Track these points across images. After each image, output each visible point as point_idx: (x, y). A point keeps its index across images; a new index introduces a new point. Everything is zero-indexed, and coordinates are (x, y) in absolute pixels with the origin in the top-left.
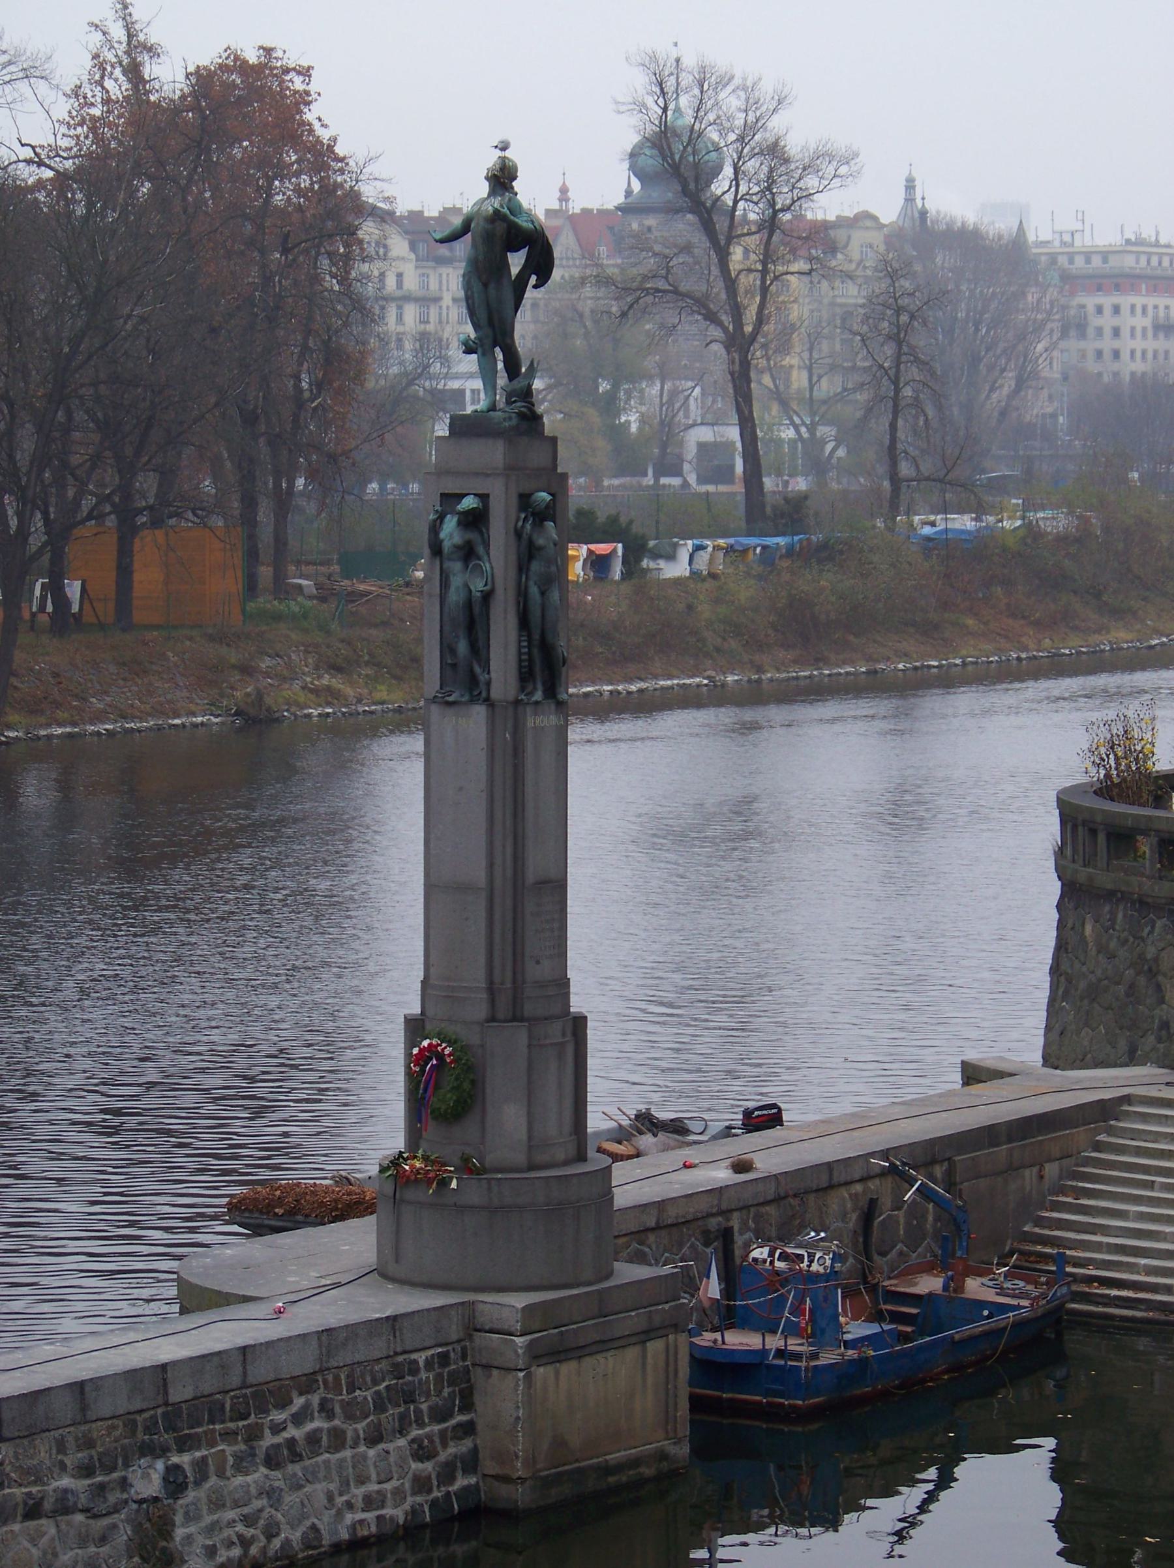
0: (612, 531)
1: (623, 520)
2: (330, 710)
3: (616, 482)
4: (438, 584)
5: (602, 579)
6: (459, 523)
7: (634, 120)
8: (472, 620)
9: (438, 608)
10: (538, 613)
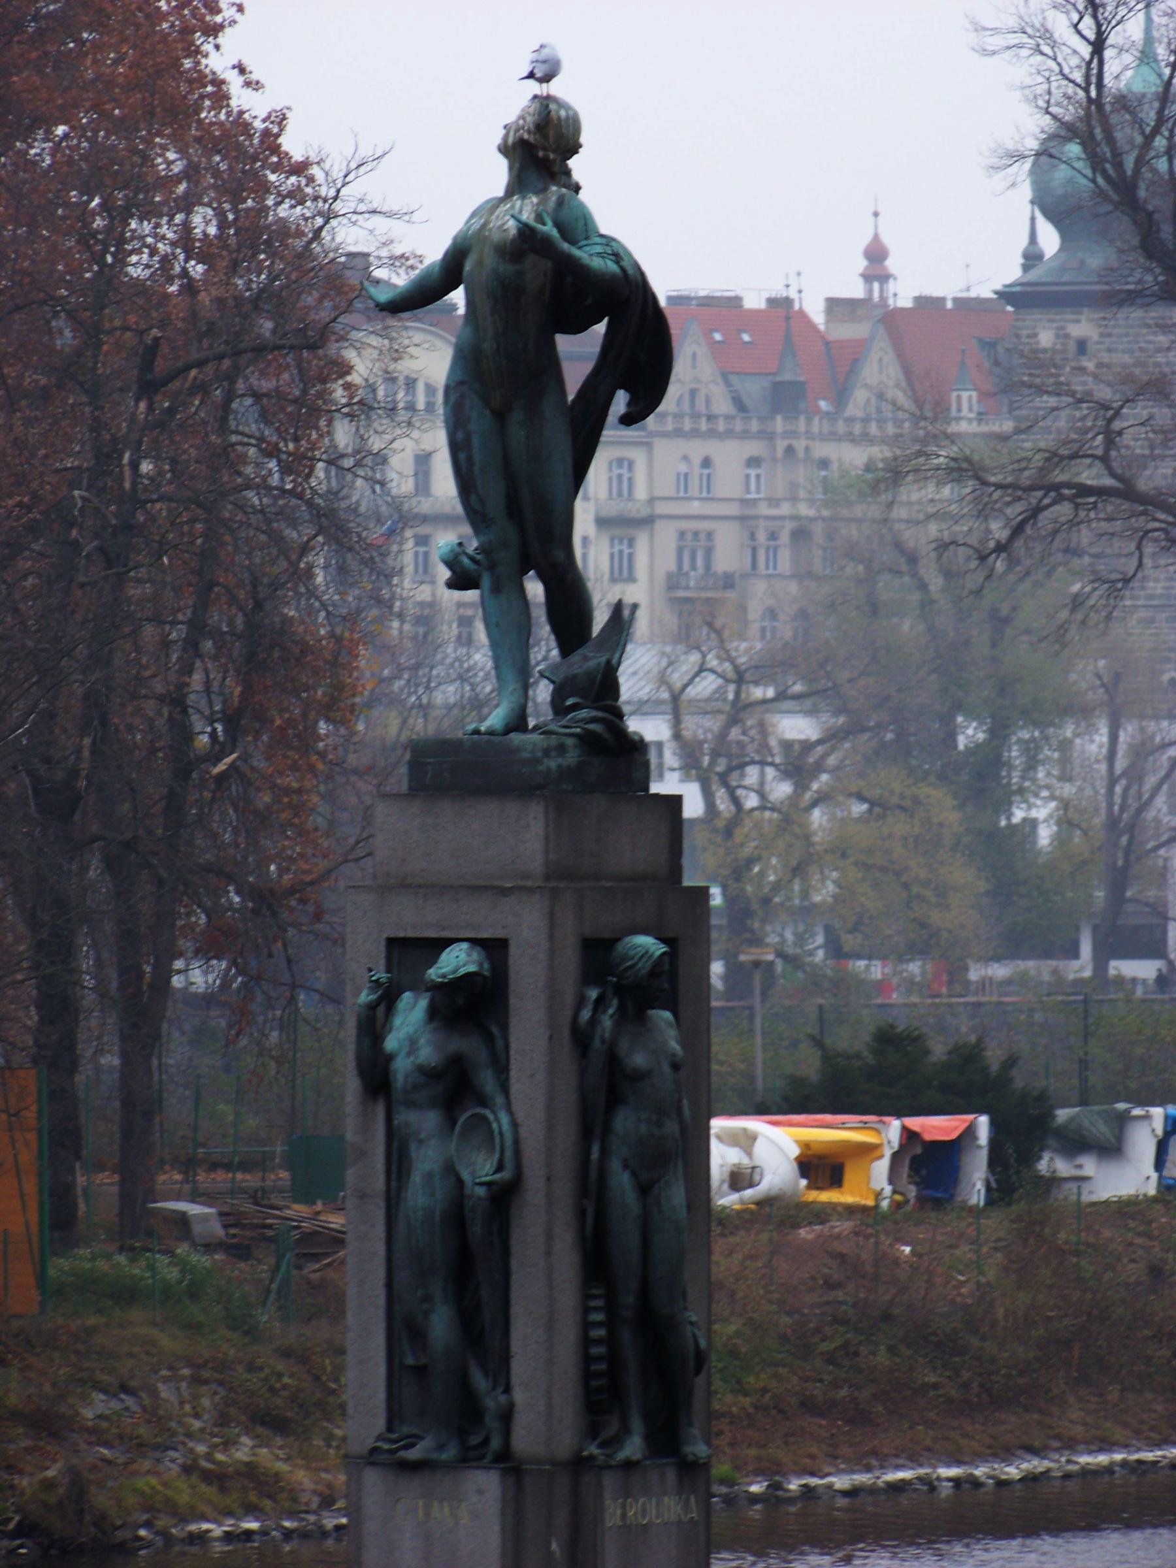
0: (964, 1083)
1: (994, 1056)
2: (254, 1525)
3: (1000, 971)
4: (380, 1166)
5: (938, 1204)
6: (433, 1013)
7: (1024, 70)
8: (465, 1254)
9: (380, 1231)
10: (632, 1239)
